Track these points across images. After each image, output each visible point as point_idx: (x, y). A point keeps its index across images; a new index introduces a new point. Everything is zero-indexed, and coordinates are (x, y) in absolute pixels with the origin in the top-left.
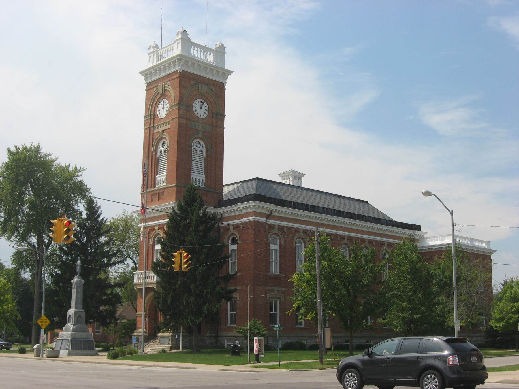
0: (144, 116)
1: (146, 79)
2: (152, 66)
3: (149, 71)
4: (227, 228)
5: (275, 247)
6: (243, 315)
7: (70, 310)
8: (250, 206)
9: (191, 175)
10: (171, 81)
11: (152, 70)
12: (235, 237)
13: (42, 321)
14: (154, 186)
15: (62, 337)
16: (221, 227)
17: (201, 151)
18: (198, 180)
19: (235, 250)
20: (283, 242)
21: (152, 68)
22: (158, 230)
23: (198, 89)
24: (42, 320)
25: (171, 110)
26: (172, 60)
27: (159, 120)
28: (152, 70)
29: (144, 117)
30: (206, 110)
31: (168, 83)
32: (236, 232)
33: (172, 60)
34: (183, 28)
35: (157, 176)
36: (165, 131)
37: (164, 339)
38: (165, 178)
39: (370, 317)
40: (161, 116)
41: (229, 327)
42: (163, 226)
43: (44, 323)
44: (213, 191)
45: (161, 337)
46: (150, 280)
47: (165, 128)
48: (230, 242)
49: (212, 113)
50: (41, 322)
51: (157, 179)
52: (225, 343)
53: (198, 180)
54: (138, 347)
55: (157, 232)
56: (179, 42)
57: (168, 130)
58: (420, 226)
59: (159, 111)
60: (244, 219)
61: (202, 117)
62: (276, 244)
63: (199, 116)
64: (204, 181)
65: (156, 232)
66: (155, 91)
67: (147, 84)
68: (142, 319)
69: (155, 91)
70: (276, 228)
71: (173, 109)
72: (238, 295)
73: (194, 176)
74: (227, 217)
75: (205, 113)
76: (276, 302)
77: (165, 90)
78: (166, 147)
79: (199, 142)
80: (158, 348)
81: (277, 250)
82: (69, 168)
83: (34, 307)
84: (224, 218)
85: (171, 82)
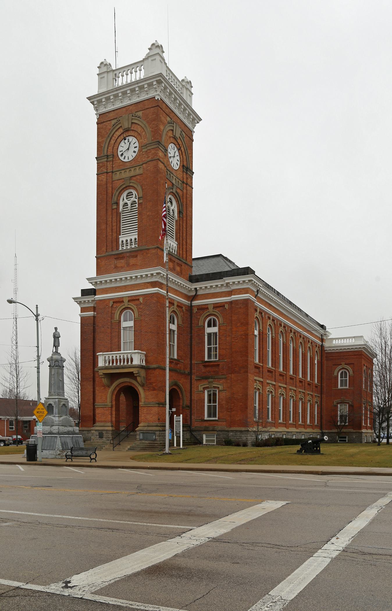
0: (96, 158)
1: (96, 109)
4: (203, 308)
5: (256, 333)
6: (232, 407)
8: (89, 301)
10: (143, 111)
13: (39, 410)
14: (118, 249)
19: (215, 334)
20: (261, 328)
22: (128, 303)
23: (172, 130)
24: (39, 409)
25: (143, 150)
27: (121, 163)
29: (96, 159)
31: (137, 114)
35: (120, 236)
36: (134, 178)
40: (124, 158)
42: (138, 298)
43: (40, 414)
44: (184, 261)
47: (132, 173)
49: (183, 166)
50: (37, 412)
51: (121, 240)
52: (202, 438)
54: (113, 444)
55: (126, 306)
56: (104, 77)
57: (138, 177)
59: (120, 152)
60: (233, 296)
65: (124, 305)
66: (113, 125)
67: (99, 115)
68: (347, 407)
69: (113, 125)
71: (148, 148)
77: (132, 123)
80: (143, 445)
84: (198, 295)
85: (143, 113)
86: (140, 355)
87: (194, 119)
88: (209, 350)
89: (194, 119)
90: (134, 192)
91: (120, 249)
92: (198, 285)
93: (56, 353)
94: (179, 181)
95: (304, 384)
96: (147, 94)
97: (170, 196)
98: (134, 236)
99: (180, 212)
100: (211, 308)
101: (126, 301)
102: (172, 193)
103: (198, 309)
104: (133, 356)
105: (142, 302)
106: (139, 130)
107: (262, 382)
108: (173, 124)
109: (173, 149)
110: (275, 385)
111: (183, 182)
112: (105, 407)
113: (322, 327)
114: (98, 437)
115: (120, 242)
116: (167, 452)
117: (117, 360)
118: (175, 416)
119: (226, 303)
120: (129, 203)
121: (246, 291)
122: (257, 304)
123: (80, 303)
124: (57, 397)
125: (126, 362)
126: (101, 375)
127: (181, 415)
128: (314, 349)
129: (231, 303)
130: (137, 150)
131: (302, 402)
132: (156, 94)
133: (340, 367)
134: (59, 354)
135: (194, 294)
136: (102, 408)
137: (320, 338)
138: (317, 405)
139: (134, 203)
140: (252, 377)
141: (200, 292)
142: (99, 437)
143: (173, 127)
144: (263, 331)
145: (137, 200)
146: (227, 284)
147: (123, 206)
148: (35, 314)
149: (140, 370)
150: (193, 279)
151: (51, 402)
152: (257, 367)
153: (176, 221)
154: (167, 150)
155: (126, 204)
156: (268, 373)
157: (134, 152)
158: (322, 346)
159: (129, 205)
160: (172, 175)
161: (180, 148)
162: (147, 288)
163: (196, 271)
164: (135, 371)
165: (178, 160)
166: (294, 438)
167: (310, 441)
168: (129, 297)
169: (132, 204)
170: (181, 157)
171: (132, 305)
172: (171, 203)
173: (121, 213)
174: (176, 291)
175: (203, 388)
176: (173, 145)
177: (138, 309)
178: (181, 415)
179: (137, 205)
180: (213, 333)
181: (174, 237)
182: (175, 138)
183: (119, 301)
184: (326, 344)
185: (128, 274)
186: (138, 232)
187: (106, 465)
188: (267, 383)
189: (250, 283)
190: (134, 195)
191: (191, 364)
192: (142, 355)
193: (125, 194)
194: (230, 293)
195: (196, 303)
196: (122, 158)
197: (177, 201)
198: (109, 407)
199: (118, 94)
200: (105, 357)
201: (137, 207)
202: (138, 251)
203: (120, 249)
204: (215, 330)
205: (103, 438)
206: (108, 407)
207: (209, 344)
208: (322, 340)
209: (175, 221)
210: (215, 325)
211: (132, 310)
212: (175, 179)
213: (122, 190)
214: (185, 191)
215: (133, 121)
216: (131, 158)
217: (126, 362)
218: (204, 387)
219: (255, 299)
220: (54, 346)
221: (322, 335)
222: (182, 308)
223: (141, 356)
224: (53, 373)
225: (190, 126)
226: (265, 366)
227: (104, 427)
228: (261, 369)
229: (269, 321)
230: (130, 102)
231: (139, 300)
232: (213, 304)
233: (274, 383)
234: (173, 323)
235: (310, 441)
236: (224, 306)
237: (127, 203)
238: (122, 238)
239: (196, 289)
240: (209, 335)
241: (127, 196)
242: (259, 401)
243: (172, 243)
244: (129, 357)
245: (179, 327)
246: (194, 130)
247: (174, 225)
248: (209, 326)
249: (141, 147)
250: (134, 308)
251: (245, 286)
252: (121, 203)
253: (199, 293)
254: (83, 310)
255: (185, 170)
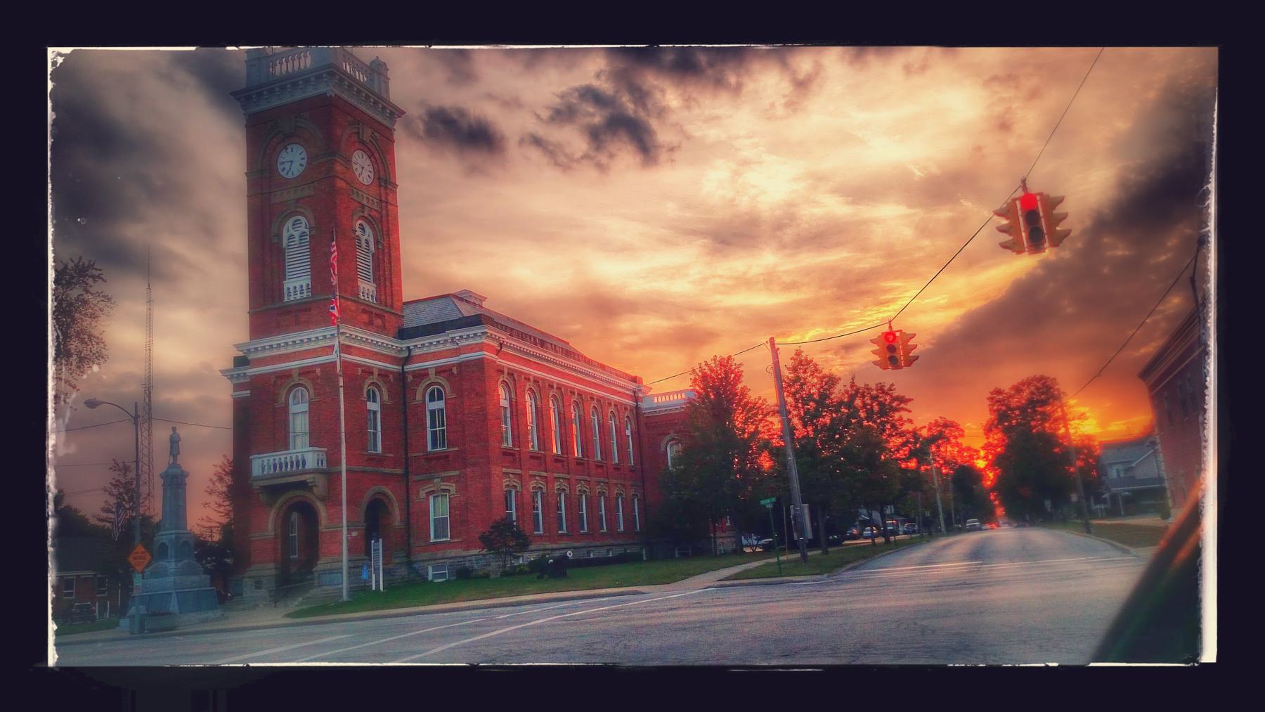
2: (1106, 48)
3: (314, 74)
4: (422, 375)
7: (160, 533)
8: (317, 338)
11: (323, 71)
12: (438, 389)
16: (407, 372)
19: (442, 410)
23: (358, 133)
24: (137, 553)
28: (323, 71)
32: (440, 380)
39: (762, 501)
41: (434, 544)
46: (295, 468)
48: (427, 399)
52: (427, 572)
53: (298, 289)
55: (297, 381)
58: (235, 358)
60: (462, 356)
70: (432, 372)
72: (454, 485)
74: (416, 356)
75: (301, 165)
76: (510, 492)
82: (93, 269)
83: (342, 555)
84: (413, 356)
86: (317, 453)
87: (392, 113)
88: (434, 433)
89: (392, 113)
90: (303, 220)
91: (286, 300)
92: (411, 343)
93: (175, 464)
94: (374, 200)
95: (605, 470)
97: (360, 222)
98: (305, 281)
99: (377, 242)
100: (432, 372)
101: (295, 375)
102: (363, 218)
103: (414, 377)
104: (306, 455)
107: (520, 476)
108: (358, 125)
109: (361, 156)
110: (546, 477)
111: (381, 201)
113: (634, 379)
114: (254, 587)
115: (285, 291)
116: (345, 600)
117: (292, 463)
119: (453, 365)
120: (297, 234)
121: (481, 347)
122: (501, 362)
123: (231, 377)
124: (173, 532)
125: (295, 466)
126: (257, 489)
127: (381, 540)
128: (621, 414)
129: (460, 365)
130: (304, 162)
131: (605, 497)
132: (327, 88)
133: (668, 438)
134: (179, 467)
135: (405, 354)
137: (632, 396)
138: (638, 500)
139: (303, 235)
140: (496, 470)
141: (416, 352)
143: (358, 128)
144: (516, 400)
145: (307, 231)
146: (453, 338)
147: (289, 239)
148: (133, 416)
149: (318, 476)
150: (403, 334)
151: (164, 541)
152: (507, 453)
153: (373, 255)
154: (350, 161)
155: (292, 237)
156: (532, 461)
157: (301, 165)
158: (637, 407)
159: (297, 238)
160: (361, 193)
161: (373, 154)
163: (412, 319)
164: (308, 478)
165: (370, 171)
166: (592, 556)
167: (551, 561)
168: (299, 368)
169: (301, 236)
170: (375, 166)
171: (304, 381)
172: (363, 229)
173: (284, 249)
174: (376, 353)
175: (427, 493)
176: (360, 153)
178: (381, 540)
179: (308, 237)
180: (439, 410)
181: (372, 278)
182: (363, 143)
183: (286, 375)
184: (644, 405)
186: (311, 275)
188: (531, 476)
189: (484, 337)
190: (304, 223)
191: (407, 459)
192: (320, 454)
193: (289, 223)
194: (458, 352)
195: (408, 368)
196: (283, 174)
197: (372, 228)
200: (263, 461)
201: (308, 240)
202: (310, 302)
203: (286, 300)
204: (439, 405)
205: (261, 588)
207: (433, 425)
208: (636, 399)
209: (370, 255)
210: (440, 398)
211: (306, 388)
212: (367, 198)
213: (286, 216)
214: (384, 212)
216: (296, 174)
217: (295, 466)
218: (426, 491)
219: (497, 357)
220: (171, 453)
221: (634, 392)
222: (388, 376)
223: (318, 455)
224: (168, 496)
225: (387, 123)
226: (523, 450)
228: (517, 456)
229: (528, 384)
231: (315, 372)
232: (435, 367)
233: (544, 474)
234: (374, 401)
235: (551, 561)
236: (451, 370)
237: (293, 235)
238: (289, 284)
239: (409, 347)
240: (433, 412)
241: (294, 225)
242: (517, 505)
243: (367, 287)
244: (300, 458)
245: (383, 405)
246: (395, 127)
247: (371, 261)
248: (432, 399)
249: (311, 158)
250: (309, 385)
251: (478, 341)
252: (285, 235)
253: (413, 353)
254: (237, 387)
255: (382, 184)
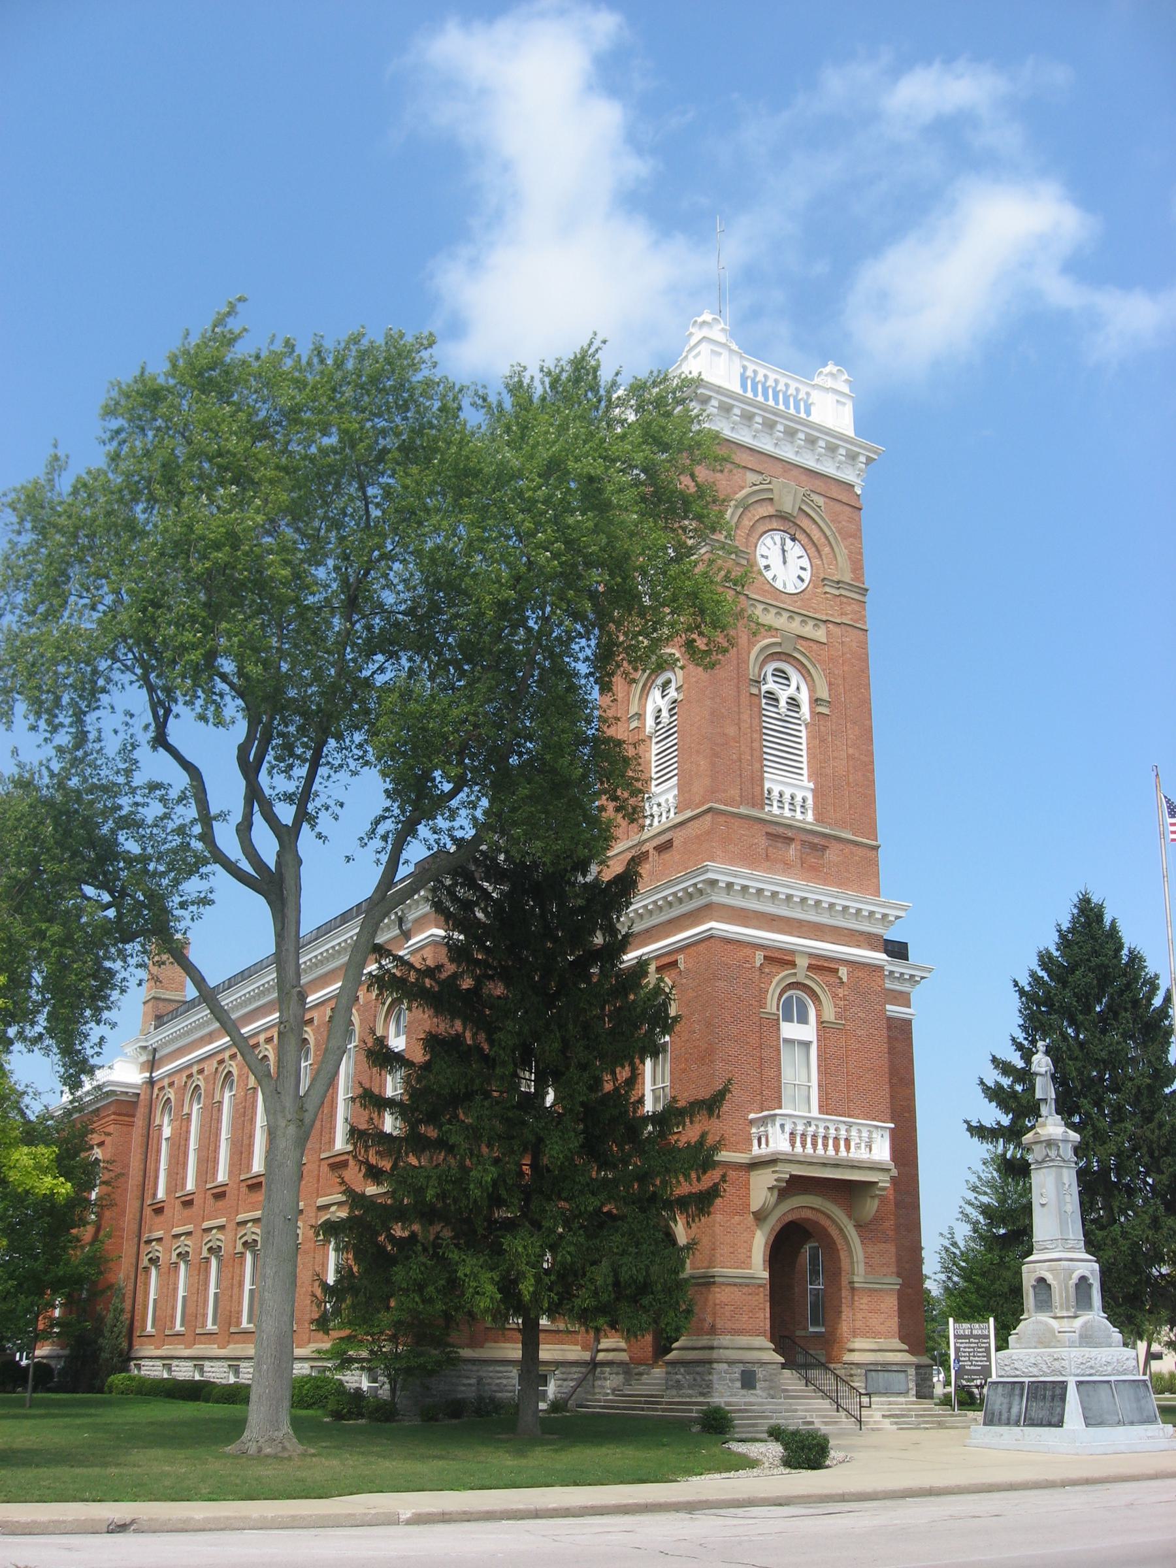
9: (762, 779)
15: (1093, 1371)
17: (793, 703)
18: (787, 797)
21: (718, 392)
26: (849, 446)
30: (802, 568)
33: (849, 446)
34: (245, 330)
37: (886, 1374)
38: (675, 796)
45: (872, 1368)
53: (787, 797)
61: (791, 589)
62: (803, 1019)
63: (779, 585)
64: (810, 802)
65: (795, 974)
70: (802, 962)
73: (775, 782)
77: (800, 509)
78: (672, 693)
79: (784, 672)
81: (806, 1045)
96: (797, 452)
100: (802, 962)
105: (845, 979)
106: (816, 535)
112: (747, 1285)
114: (738, 1384)
118: (951, 1320)
127: (991, 1320)
136: (735, 1288)
142: (743, 1387)
145: (804, 698)
162: (858, 946)
168: (811, 955)
177: (835, 995)
183: (780, 959)
185: (825, 894)
187: (662, 1500)
198: (760, 1286)
199: (776, 422)
205: (754, 1388)
206: (754, 1285)
215: (804, 507)
227: (741, 1352)
230: (751, 441)
